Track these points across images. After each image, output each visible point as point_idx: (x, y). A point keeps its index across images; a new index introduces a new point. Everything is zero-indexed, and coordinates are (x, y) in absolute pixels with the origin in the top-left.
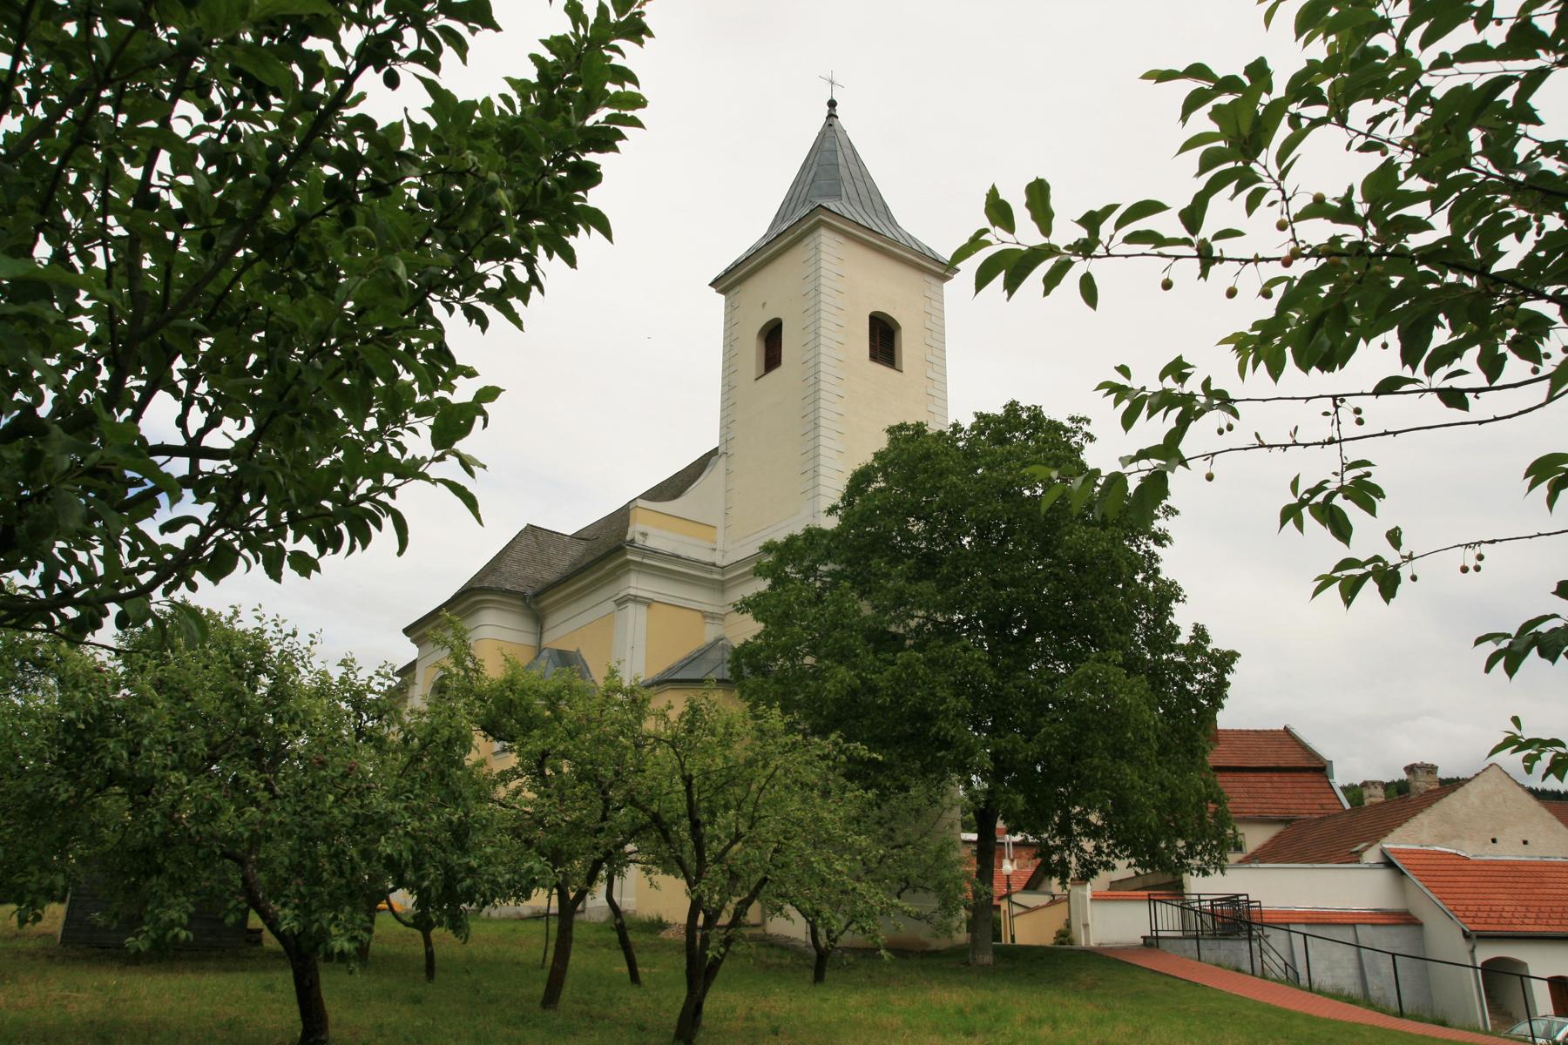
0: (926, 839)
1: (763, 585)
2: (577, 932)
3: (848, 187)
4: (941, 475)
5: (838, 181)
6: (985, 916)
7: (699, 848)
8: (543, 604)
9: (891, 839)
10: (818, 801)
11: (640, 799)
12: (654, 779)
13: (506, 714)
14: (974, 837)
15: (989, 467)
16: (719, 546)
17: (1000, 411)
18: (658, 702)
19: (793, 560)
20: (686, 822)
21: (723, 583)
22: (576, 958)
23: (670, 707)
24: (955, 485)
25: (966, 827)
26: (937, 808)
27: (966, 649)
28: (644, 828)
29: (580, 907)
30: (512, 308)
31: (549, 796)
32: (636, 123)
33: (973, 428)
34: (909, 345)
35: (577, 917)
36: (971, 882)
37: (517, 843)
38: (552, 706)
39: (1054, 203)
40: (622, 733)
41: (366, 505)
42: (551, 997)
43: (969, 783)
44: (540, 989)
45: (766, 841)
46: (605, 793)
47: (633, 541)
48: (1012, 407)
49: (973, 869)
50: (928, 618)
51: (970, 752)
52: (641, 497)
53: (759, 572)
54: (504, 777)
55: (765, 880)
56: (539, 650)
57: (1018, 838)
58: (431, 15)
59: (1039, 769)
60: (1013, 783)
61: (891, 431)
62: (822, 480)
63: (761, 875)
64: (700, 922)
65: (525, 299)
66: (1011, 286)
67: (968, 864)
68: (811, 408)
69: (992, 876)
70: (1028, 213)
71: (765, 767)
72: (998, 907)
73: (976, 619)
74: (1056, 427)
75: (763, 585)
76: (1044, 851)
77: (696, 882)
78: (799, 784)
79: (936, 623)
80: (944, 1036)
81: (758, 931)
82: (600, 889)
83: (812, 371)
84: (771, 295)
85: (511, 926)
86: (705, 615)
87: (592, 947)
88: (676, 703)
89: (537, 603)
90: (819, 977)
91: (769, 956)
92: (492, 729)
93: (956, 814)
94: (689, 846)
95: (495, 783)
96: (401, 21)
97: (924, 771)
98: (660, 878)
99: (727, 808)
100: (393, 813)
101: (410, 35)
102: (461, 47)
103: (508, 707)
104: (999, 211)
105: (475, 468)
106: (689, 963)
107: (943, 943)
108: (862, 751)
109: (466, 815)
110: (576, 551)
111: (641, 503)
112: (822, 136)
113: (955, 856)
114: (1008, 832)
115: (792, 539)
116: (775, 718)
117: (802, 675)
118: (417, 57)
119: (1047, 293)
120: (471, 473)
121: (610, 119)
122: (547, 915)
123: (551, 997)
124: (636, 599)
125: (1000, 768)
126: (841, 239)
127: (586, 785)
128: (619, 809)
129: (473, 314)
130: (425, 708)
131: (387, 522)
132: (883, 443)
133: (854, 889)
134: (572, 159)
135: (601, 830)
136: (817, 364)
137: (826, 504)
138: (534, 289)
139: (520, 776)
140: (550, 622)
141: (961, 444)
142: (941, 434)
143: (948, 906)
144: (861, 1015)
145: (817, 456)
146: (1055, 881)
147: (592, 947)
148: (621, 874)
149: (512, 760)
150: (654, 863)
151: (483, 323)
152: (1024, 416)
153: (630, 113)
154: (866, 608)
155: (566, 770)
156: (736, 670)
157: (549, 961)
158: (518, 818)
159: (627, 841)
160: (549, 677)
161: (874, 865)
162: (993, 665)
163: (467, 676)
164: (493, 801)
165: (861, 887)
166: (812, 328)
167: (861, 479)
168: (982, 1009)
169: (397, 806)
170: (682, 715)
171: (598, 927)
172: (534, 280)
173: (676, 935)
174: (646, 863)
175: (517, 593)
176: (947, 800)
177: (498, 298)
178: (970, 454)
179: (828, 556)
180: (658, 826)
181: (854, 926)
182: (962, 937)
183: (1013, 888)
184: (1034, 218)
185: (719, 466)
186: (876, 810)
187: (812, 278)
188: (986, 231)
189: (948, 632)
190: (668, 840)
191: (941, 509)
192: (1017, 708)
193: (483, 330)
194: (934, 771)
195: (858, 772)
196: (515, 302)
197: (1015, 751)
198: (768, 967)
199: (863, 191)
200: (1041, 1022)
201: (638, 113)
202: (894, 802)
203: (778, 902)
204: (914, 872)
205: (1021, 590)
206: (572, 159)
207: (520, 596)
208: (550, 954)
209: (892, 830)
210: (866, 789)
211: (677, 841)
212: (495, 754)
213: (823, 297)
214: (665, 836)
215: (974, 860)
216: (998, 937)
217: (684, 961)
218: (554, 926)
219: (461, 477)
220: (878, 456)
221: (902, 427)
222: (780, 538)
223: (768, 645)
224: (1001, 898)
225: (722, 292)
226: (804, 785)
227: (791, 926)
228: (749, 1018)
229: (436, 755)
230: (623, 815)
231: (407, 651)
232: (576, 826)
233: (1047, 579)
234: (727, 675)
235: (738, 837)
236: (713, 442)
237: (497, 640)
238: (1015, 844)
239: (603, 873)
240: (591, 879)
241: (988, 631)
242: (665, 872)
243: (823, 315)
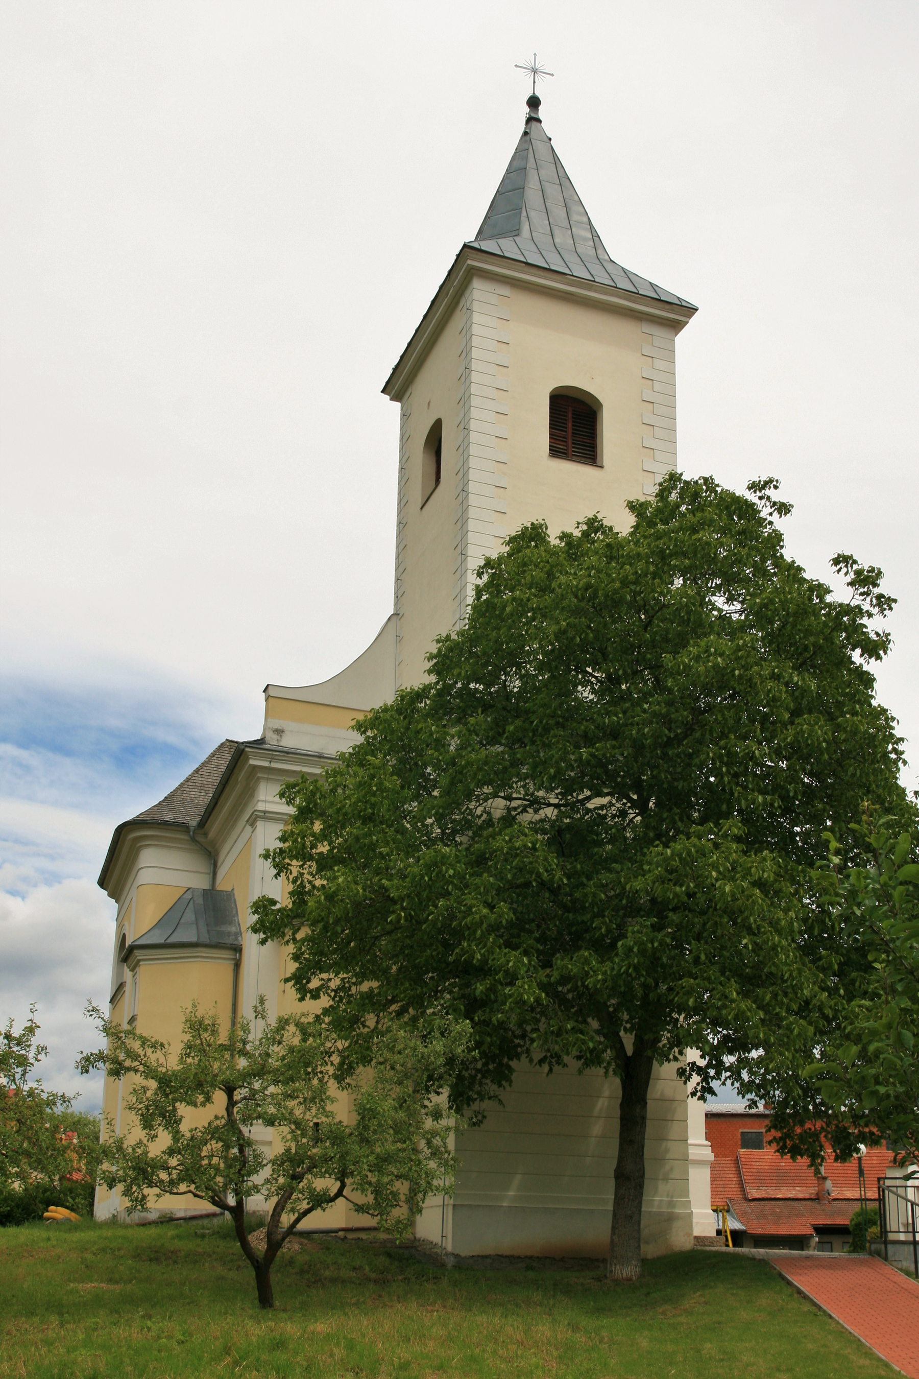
89: (206, 834)
126: (505, 291)
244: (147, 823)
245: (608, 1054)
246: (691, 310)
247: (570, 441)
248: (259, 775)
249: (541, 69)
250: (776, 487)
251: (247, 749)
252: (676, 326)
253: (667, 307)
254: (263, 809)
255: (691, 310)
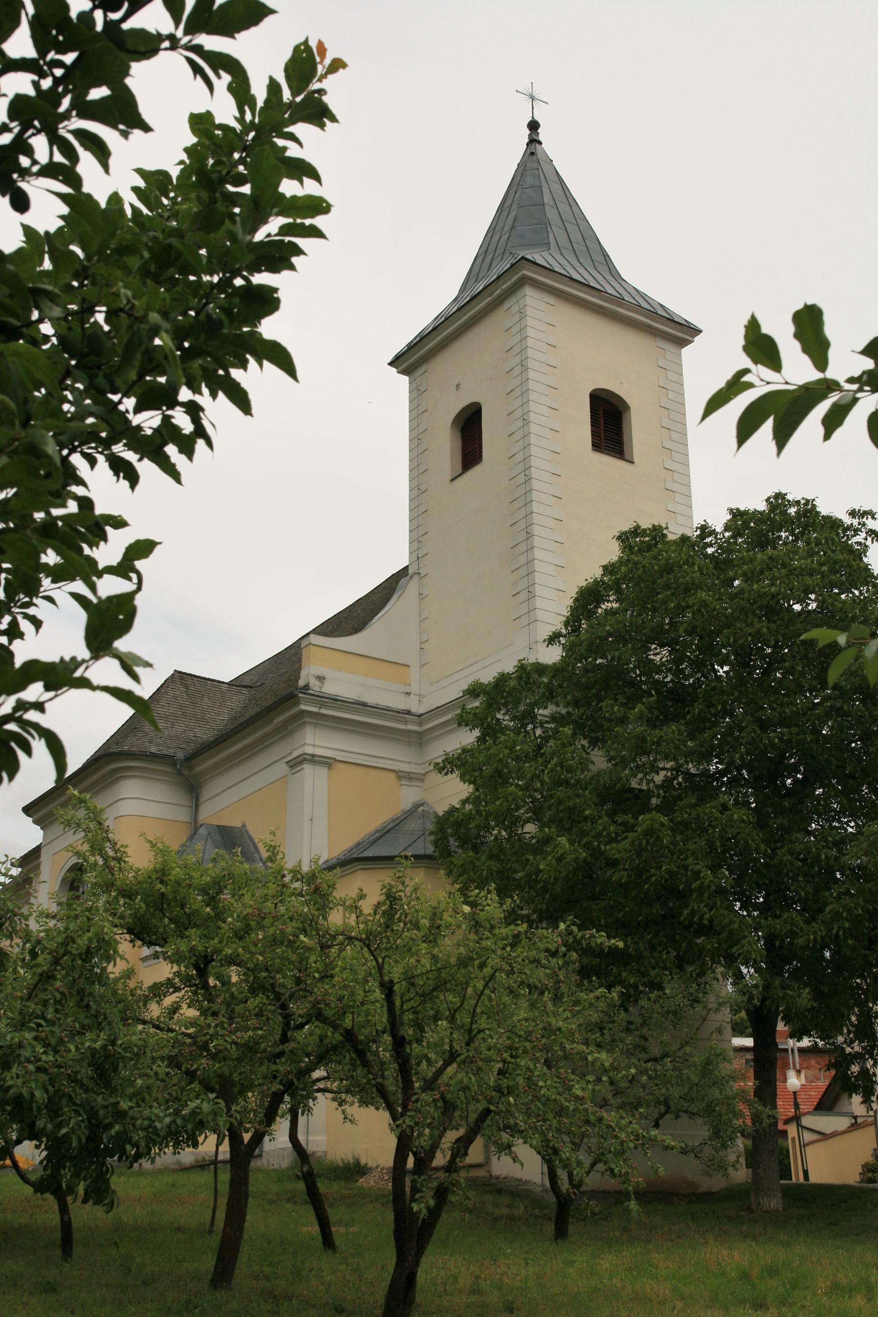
0: (687, 1049)
1: (468, 737)
2: (255, 1184)
3: (557, 234)
4: (687, 590)
5: (545, 225)
6: (769, 1147)
7: (405, 1071)
8: (198, 769)
9: (644, 1050)
10: (550, 1006)
11: (329, 1013)
12: (346, 987)
13: (157, 911)
14: (749, 1042)
15: (747, 578)
16: (414, 689)
17: (762, 506)
18: (347, 887)
19: (505, 705)
20: (387, 1038)
21: (420, 735)
22: (255, 1219)
23: (362, 897)
24: (705, 604)
25: (739, 1031)
26: (698, 1008)
27: (724, 808)
28: (335, 1048)
29: (257, 1152)
30: (167, 458)
31: (215, 1014)
32: (315, 233)
33: (727, 528)
34: (640, 429)
35: (254, 1164)
36: (745, 1101)
37: (176, 1076)
38: (212, 901)
39: (830, 330)
40: (304, 931)
41: (12, 727)
42: (223, 1273)
43: (739, 976)
44: (209, 1262)
45: (488, 1060)
46: (284, 1007)
47: (307, 687)
48: (778, 501)
49: (750, 1084)
50: (677, 770)
51: (734, 939)
52: (315, 631)
53: (464, 720)
54: (157, 991)
55: (488, 1112)
56: (195, 826)
57: (806, 1042)
58: (66, 116)
59: (827, 954)
60: (796, 975)
61: (623, 538)
62: (539, 603)
63: (481, 1106)
64: (410, 1162)
65: (188, 450)
66: (782, 437)
67: (744, 1077)
68: (520, 514)
69: (774, 1095)
70: (797, 345)
71: (482, 966)
72: (784, 1133)
73: (739, 770)
74: (833, 524)
75: (468, 737)
76: (840, 1062)
77: (402, 1115)
78: (527, 989)
79: (688, 775)
80: (726, 1309)
81: (481, 1173)
82: (282, 1127)
83: (521, 468)
84: (465, 375)
85: (169, 1179)
86: (400, 775)
87: (272, 1202)
88: (367, 889)
89: (190, 768)
90: (561, 1232)
91: (496, 1205)
92: (141, 932)
93: (725, 1014)
94: (392, 1071)
95: (146, 1000)
96: (26, 126)
97: (681, 963)
98: (355, 1109)
99: (436, 1018)
100: (20, 1046)
101: (40, 144)
102: (101, 152)
103: (159, 903)
104: (761, 347)
105: (139, 670)
106: (397, 1220)
107: (716, 1183)
108: (601, 939)
109: (113, 1043)
110: (236, 701)
111: (315, 639)
112: (523, 169)
113: (725, 1068)
114: (792, 1036)
115: (503, 678)
116: (493, 907)
117: (522, 847)
118: (50, 170)
119: (827, 436)
120: (135, 677)
121: (284, 230)
122: (215, 1162)
123: (223, 1273)
124: (313, 759)
125: (776, 956)
126: (551, 300)
127: (260, 999)
128: (301, 1026)
129: (121, 468)
130: (54, 908)
131: (39, 746)
132: (613, 552)
133: (600, 1119)
134: (239, 282)
135: (281, 1054)
136: (527, 458)
137: (545, 632)
138: (200, 444)
139: (177, 989)
140: (208, 792)
141: (710, 551)
142: (684, 539)
143: (720, 1135)
144: (617, 1282)
145: (531, 573)
146: (857, 1099)
147: (272, 1202)
148: (308, 1110)
149: (164, 971)
150: (348, 1092)
151: (133, 478)
152: (792, 511)
153: (308, 222)
154: (599, 761)
155: (234, 979)
156: (440, 842)
157: (220, 1224)
158: (177, 1043)
159: (314, 1067)
160: (206, 861)
161: (624, 1085)
162: (761, 825)
163: (106, 865)
164: (144, 1022)
165: (610, 1117)
166: (518, 414)
167: (588, 598)
168: (773, 1272)
169: (29, 1036)
170: (378, 906)
171: (280, 1176)
172: (200, 432)
173: (378, 1182)
174: (339, 1092)
175: (164, 756)
176: (711, 998)
177: (152, 448)
178: (721, 564)
179: (550, 696)
180: (354, 1046)
181: (601, 1167)
182: (741, 1175)
183: (803, 1108)
184: (805, 350)
185: (409, 593)
186: (623, 1014)
187: (516, 350)
188: (746, 371)
189: (703, 787)
190: (365, 1063)
191: (689, 633)
192: (794, 879)
193: (133, 486)
194: (692, 963)
195: (596, 967)
196: (171, 450)
197: (793, 935)
198: (495, 1220)
199: (576, 236)
200: (852, 1291)
201: (319, 221)
202: (643, 1003)
203: (505, 1137)
204: (675, 1092)
205: (794, 730)
206: (239, 282)
207: (170, 760)
208: (221, 1215)
209: (645, 1039)
210: (609, 988)
211: (379, 1067)
212: (144, 959)
213: (531, 374)
214: (362, 1054)
215: (751, 1073)
216: (786, 1173)
217: (391, 1217)
218: (225, 1176)
219: (124, 682)
220: (608, 569)
221: (636, 531)
222: (487, 677)
223: (479, 812)
224: (787, 1122)
225: (404, 372)
226: (531, 988)
227: (524, 1165)
228: (475, 1290)
229: (71, 971)
230: (307, 1035)
231: (30, 835)
232: (250, 1049)
233: (828, 715)
234: (430, 849)
235: (451, 1057)
236: (401, 560)
237: (142, 819)
238: (801, 1050)
239: (284, 1107)
240: (270, 1117)
241: (756, 782)
242: (364, 1103)
243: (532, 396)
244: (135, 755)
245: (98, 999)
246: (697, 331)
247: (603, 437)
248: (306, 719)
249: (537, 97)
250: (873, 518)
251: (300, 695)
252: (683, 343)
253: (678, 327)
254: (311, 752)
255: (697, 331)
